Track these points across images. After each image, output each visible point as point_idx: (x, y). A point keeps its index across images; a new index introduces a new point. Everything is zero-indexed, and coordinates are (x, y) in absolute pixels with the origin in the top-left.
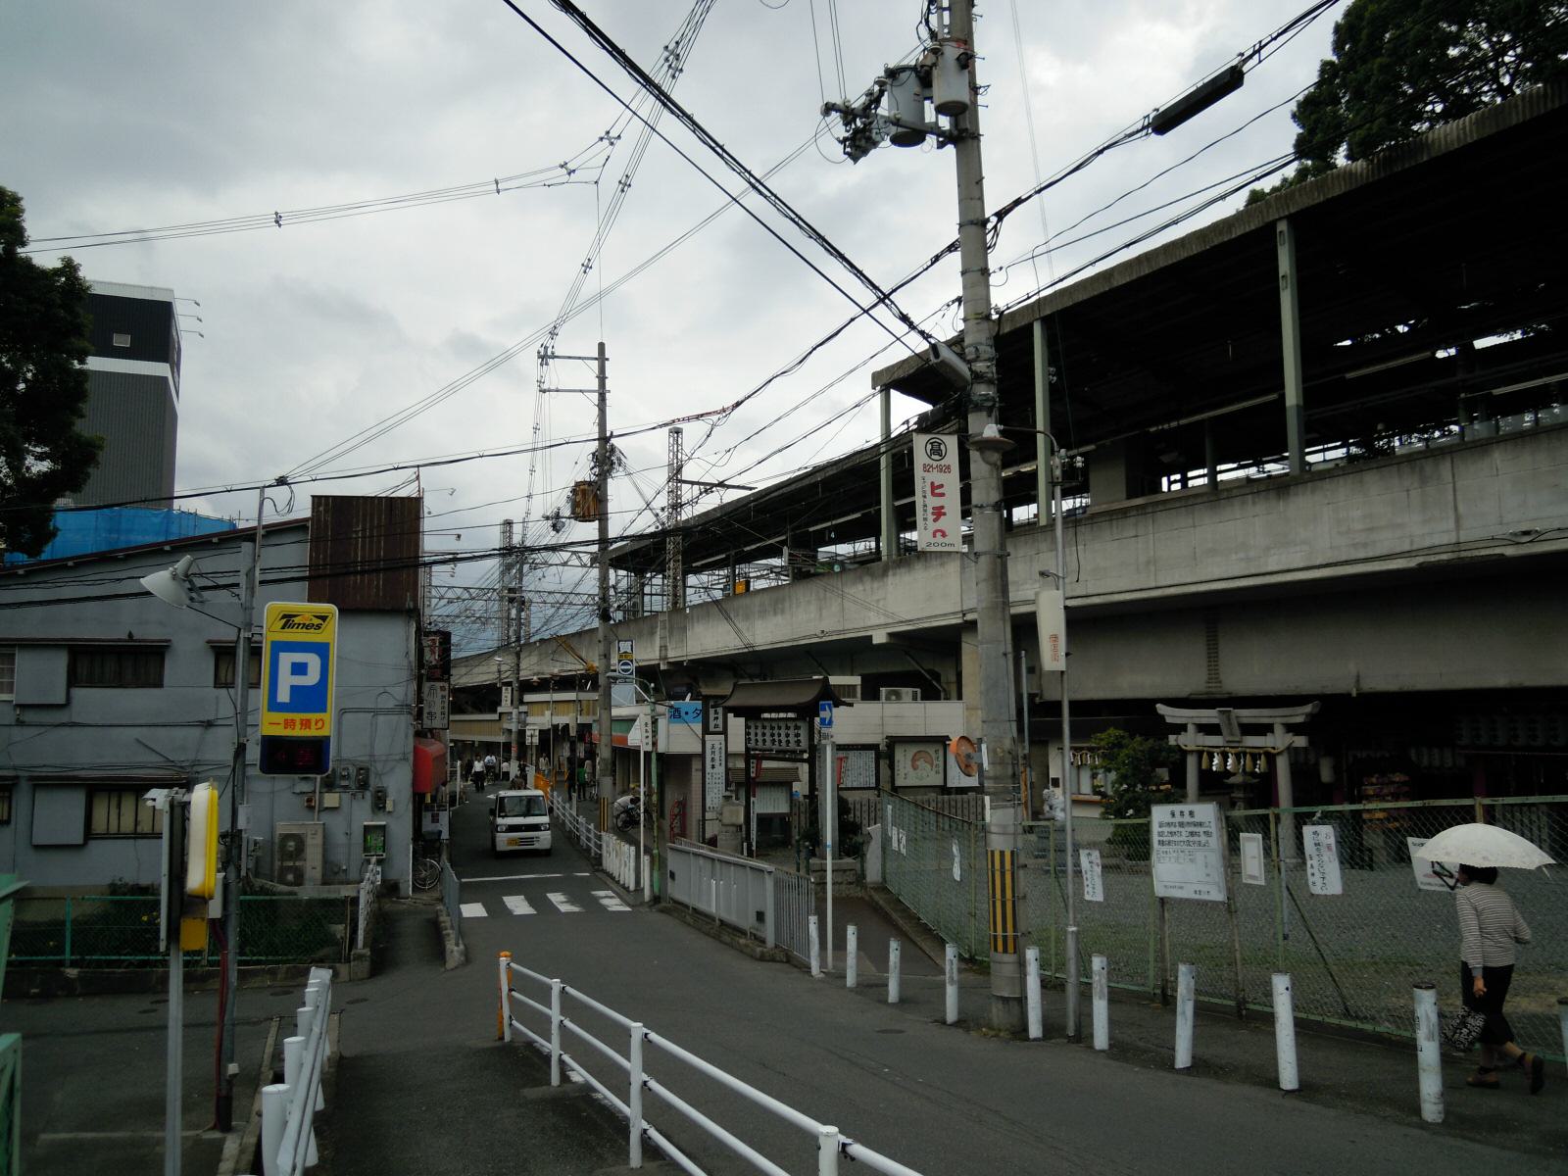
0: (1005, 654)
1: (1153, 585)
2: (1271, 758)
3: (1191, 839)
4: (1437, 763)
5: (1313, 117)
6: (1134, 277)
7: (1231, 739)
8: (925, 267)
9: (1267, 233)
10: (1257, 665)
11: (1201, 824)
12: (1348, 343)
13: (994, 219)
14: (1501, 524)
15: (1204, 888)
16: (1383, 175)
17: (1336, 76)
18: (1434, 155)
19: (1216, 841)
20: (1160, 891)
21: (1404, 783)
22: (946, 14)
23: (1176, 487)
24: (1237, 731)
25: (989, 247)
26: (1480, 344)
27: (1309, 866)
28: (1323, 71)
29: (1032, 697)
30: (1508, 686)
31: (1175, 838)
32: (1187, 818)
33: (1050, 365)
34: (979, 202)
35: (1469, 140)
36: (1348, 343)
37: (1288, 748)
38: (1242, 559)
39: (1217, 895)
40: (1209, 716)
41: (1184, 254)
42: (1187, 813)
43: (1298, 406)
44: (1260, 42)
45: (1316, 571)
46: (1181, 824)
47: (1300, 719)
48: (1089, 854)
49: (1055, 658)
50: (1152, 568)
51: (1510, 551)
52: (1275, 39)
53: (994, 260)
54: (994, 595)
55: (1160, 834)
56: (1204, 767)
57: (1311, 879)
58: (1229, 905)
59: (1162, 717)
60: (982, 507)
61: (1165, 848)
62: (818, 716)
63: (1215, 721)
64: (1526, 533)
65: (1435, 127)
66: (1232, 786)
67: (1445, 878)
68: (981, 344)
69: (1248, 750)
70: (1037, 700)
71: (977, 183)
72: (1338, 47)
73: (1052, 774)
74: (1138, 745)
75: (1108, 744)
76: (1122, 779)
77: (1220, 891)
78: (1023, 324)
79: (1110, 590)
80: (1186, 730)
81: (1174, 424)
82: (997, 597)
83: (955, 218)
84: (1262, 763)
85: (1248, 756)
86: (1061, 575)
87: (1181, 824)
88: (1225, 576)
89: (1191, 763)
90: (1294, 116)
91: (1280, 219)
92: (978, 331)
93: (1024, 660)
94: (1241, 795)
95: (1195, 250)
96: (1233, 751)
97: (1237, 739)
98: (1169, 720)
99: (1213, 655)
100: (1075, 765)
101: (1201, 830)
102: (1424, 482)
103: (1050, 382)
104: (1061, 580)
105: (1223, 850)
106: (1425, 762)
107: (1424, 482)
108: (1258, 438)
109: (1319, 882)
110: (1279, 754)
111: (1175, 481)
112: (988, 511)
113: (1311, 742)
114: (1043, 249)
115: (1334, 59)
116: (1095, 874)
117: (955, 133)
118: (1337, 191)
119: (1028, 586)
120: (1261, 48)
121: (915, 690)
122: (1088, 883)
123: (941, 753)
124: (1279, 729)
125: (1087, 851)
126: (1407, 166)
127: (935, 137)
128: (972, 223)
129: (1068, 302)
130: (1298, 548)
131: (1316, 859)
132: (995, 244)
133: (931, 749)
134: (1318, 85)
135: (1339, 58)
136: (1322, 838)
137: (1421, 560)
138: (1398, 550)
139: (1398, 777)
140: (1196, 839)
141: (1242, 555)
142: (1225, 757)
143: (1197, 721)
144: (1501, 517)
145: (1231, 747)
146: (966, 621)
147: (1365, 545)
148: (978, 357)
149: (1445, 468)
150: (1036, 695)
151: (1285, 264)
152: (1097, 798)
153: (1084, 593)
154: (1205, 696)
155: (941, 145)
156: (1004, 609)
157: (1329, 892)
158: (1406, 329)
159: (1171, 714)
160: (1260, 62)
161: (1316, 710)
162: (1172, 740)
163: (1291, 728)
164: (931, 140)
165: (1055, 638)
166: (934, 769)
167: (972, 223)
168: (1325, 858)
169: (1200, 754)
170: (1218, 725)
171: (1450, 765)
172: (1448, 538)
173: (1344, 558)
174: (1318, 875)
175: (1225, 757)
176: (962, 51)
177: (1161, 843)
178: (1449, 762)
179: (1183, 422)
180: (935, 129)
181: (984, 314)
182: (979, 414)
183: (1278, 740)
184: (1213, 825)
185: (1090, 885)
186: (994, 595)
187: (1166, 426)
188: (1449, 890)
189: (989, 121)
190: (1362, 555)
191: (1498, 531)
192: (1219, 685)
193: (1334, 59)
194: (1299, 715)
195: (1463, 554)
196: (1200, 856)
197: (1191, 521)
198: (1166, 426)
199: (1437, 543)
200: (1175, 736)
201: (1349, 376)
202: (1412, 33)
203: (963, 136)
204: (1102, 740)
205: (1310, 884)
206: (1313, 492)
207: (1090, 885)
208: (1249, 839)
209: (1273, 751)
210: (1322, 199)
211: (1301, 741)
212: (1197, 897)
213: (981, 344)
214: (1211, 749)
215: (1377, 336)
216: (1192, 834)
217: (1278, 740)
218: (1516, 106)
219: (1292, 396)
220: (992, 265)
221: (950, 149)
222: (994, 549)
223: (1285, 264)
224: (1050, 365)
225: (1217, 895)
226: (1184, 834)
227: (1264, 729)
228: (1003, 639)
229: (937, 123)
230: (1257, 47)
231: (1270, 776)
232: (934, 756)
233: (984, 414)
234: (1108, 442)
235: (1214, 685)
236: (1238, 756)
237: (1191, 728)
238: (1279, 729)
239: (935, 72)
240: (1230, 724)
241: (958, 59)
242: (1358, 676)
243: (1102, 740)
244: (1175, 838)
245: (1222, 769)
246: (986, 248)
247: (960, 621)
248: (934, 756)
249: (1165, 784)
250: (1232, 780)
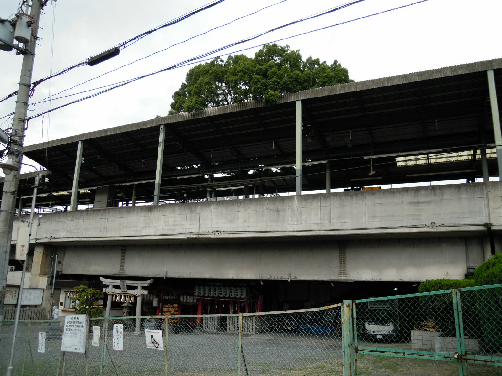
0: (6, 252)
1: (105, 236)
3: (77, 328)
4: (188, 301)
5: (177, 98)
6: (115, 133)
7: (123, 291)
8: (5, 98)
9: (157, 128)
10: (138, 266)
11: (80, 323)
12: (179, 168)
13: (33, 85)
14: (211, 228)
15: (78, 348)
16: (192, 118)
17: (186, 88)
18: (207, 116)
19: (84, 329)
20: (63, 348)
21: (177, 307)
22: (30, 8)
23: (125, 206)
24: (126, 288)
25: (30, 96)
26: (216, 175)
27: (114, 339)
28: (182, 86)
29: (58, 272)
30: (209, 278)
31: (72, 328)
32: (76, 320)
33: (83, 157)
34: (29, 78)
35: (216, 114)
36: (179, 168)
37: (142, 294)
38: (135, 230)
39: (82, 350)
40: (117, 282)
41: (131, 129)
42: (76, 318)
43: (159, 183)
44: (126, 41)
46: (74, 323)
47: (146, 285)
48: (42, 334)
49: (22, 255)
50: (106, 230)
51: (213, 236)
52: (130, 41)
53: (30, 101)
54: (5, 228)
55: (67, 326)
56: (113, 300)
57: (114, 344)
58: (86, 355)
59: (102, 282)
60: (6, 192)
61: (67, 332)
63: (119, 284)
64: (217, 231)
65: (211, 109)
66: (123, 307)
67: (155, 344)
68: (18, 130)
70: (60, 273)
71: (29, 71)
72: (187, 80)
73: (61, 301)
74: (91, 291)
75: (80, 290)
76: (82, 303)
77: (83, 349)
78: (75, 141)
79: (90, 236)
80: (137, 289)
81: (123, 184)
82: (6, 229)
83: (18, 80)
84: (132, 299)
85: (128, 297)
86: (31, 222)
87: (74, 323)
88: (129, 235)
89: (109, 298)
90: (172, 96)
91: (162, 124)
92: (18, 125)
93: (56, 258)
94: (126, 310)
95: (135, 128)
96: (124, 295)
98: (104, 283)
100: (70, 297)
101: (80, 325)
102: (191, 212)
103: (82, 163)
104: (30, 224)
105: (87, 333)
106: (185, 301)
107: (191, 212)
108: (146, 193)
109: (116, 346)
110: (138, 296)
111: (125, 204)
112: (9, 195)
113: (149, 293)
114: (48, 99)
115: (186, 83)
116: (43, 341)
117: (24, 50)
118: (179, 120)
119: (62, 232)
120: (126, 43)
121: (12, 266)
122: (40, 345)
123: (17, 291)
124: (139, 288)
125: (42, 332)
126: (199, 117)
127: (16, 50)
128: (24, 84)
129: (92, 137)
130: (153, 229)
131: (116, 336)
132: (32, 95)
133: (13, 290)
134: (180, 90)
135: (187, 83)
136: (119, 329)
137: (188, 236)
138: (182, 232)
139: (176, 305)
140: (78, 328)
141: (135, 229)
142: (121, 296)
143: (113, 284)
146: (37, 243)
147: (172, 230)
148: (16, 135)
149: (198, 209)
150: (60, 271)
151: (161, 138)
152: (74, 310)
153: (81, 237)
154: (118, 276)
155: (18, 54)
156: (8, 233)
157: (119, 349)
158: (197, 167)
159: (104, 281)
160: (125, 48)
161: (152, 282)
162: (104, 290)
163: (144, 288)
164: (14, 51)
165: (23, 247)
166: (13, 298)
167: (24, 84)
168: (119, 336)
169: (113, 295)
170: (120, 286)
171: (192, 302)
172: (197, 230)
173: (165, 233)
174: (116, 343)
175: (121, 296)
176: (29, 20)
177: (67, 330)
178: (192, 301)
179: (126, 184)
180: (18, 48)
181: (21, 119)
182: (12, 156)
183: (138, 292)
184: (84, 323)
185: (41, 346)
186: (5, 228)
187: (120, 185)
188: (155, 348)
189: (39, 50)
190: (171, 233)
191: (210, 230)
193: (186, 83)
194: (146, 283)
195: (200, 236)
196: (78, 335)
197: (120, 216)
198: (120, 185)
199: (193, 232)
200: (105, 289)
201: (178, 178)
202: (205, 80)
203: (27, 53)
204: (78, 289)
205: (113, 345)
206: (159, 211)
207: (41, 346)
208: (96, 329)
209: (137, 295)
210: (174, 121)
211: (146, 292)
212: (75, 351)
213: (18, 130)
214: (117, 294)
215: (189, 168)
216: (77, 326)
217: (138, 292)
218: (229, 108)
219: (158, 180)
220: (30, 102)
221: (22, 56)
222: (9, 209)
223: (161, 138)
224: (83, 157)
225: (82, 350)
226: (75, 326)
227: (134, 288)
228: (5, 245)
229: (18, 45)
230: (124, 43)
232: (14, 292)
233: (15, 157)
234: (101, 187)
236: (125, 297)
237: (111, 286)
238: (139, 288)
239: (18, 23)
240: (124, 286)
241: (27, 22)
242: (167, 272)
243: (78, 289)
244: (72, 328)
245: (119, 301)
246: (29, 96)
247: (34, 242)
248: (14, 292)
249: (101, 305)
250: (124, 305)
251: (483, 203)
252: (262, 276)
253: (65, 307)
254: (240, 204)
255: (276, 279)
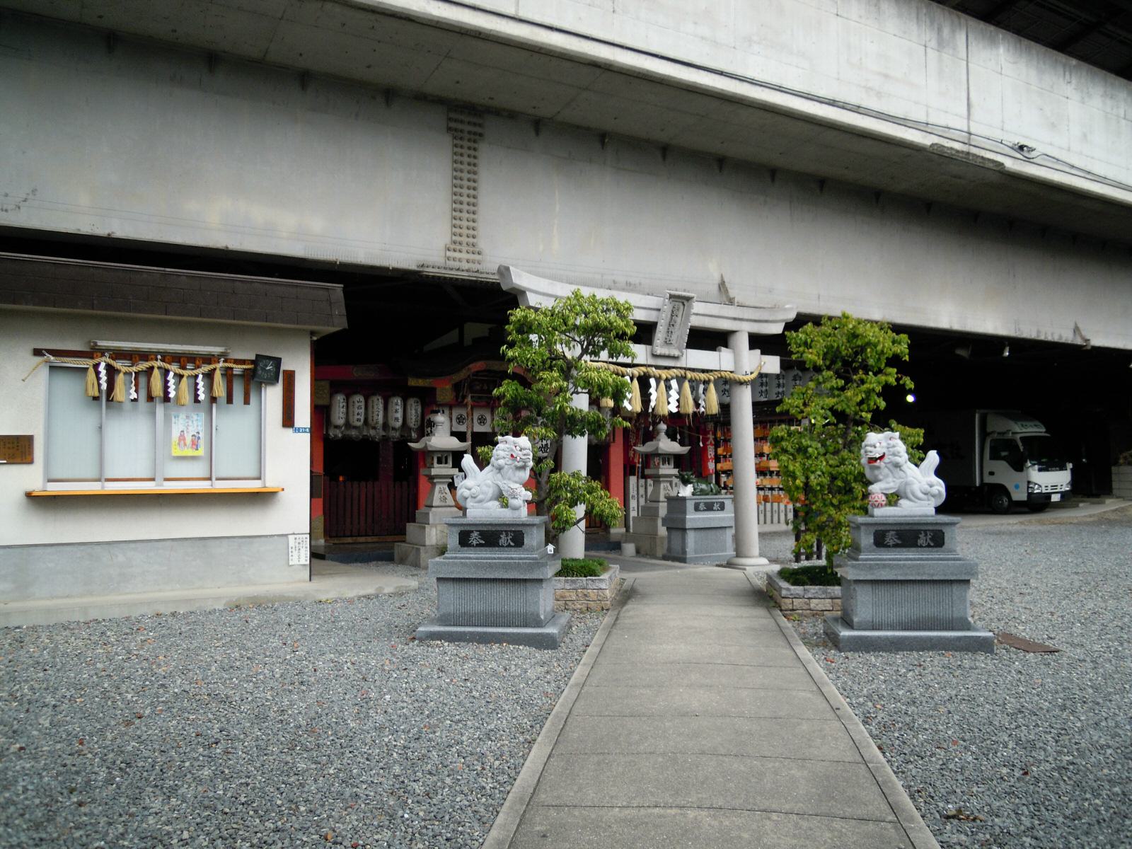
2: (727, 384)
45: (818, 104)
51: (1011, 164)
62: (508, 322)
69: (689, 375)
97: (676, 353)
99: (464, 204)
102: (941, 45)
137: (936, 140)
144: (1003, 122)
145: (657, 367)
147: (879, 95)
191: (998, 135)
192: (476, 257)
195: (974, 151)
231: (724, 418)
235: (464, 256)
251: (955, 616)
252: (1019, 330)
253: (208, 476)
254: (1071, 78)
255: (1050, 338)
